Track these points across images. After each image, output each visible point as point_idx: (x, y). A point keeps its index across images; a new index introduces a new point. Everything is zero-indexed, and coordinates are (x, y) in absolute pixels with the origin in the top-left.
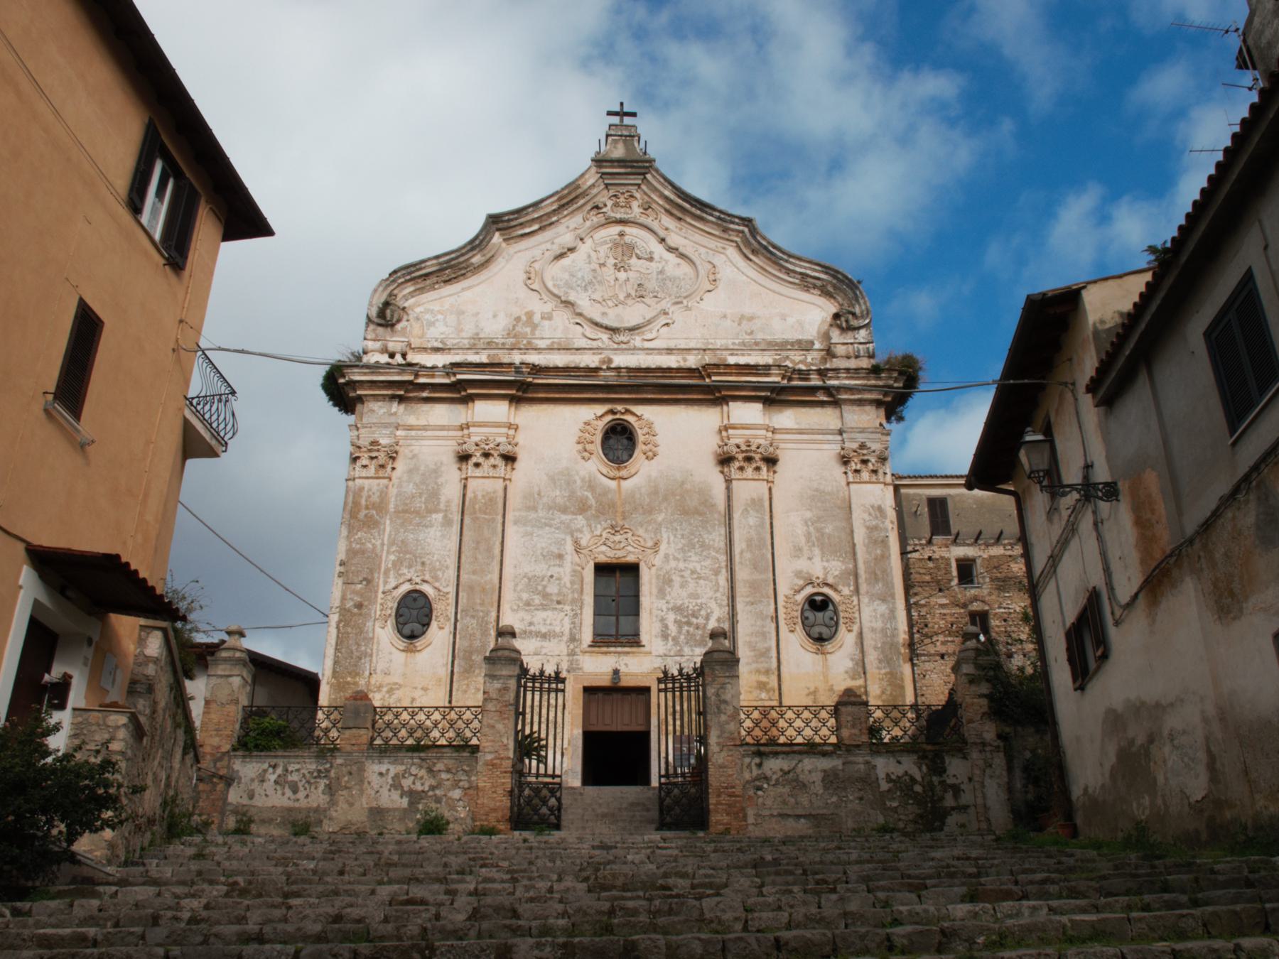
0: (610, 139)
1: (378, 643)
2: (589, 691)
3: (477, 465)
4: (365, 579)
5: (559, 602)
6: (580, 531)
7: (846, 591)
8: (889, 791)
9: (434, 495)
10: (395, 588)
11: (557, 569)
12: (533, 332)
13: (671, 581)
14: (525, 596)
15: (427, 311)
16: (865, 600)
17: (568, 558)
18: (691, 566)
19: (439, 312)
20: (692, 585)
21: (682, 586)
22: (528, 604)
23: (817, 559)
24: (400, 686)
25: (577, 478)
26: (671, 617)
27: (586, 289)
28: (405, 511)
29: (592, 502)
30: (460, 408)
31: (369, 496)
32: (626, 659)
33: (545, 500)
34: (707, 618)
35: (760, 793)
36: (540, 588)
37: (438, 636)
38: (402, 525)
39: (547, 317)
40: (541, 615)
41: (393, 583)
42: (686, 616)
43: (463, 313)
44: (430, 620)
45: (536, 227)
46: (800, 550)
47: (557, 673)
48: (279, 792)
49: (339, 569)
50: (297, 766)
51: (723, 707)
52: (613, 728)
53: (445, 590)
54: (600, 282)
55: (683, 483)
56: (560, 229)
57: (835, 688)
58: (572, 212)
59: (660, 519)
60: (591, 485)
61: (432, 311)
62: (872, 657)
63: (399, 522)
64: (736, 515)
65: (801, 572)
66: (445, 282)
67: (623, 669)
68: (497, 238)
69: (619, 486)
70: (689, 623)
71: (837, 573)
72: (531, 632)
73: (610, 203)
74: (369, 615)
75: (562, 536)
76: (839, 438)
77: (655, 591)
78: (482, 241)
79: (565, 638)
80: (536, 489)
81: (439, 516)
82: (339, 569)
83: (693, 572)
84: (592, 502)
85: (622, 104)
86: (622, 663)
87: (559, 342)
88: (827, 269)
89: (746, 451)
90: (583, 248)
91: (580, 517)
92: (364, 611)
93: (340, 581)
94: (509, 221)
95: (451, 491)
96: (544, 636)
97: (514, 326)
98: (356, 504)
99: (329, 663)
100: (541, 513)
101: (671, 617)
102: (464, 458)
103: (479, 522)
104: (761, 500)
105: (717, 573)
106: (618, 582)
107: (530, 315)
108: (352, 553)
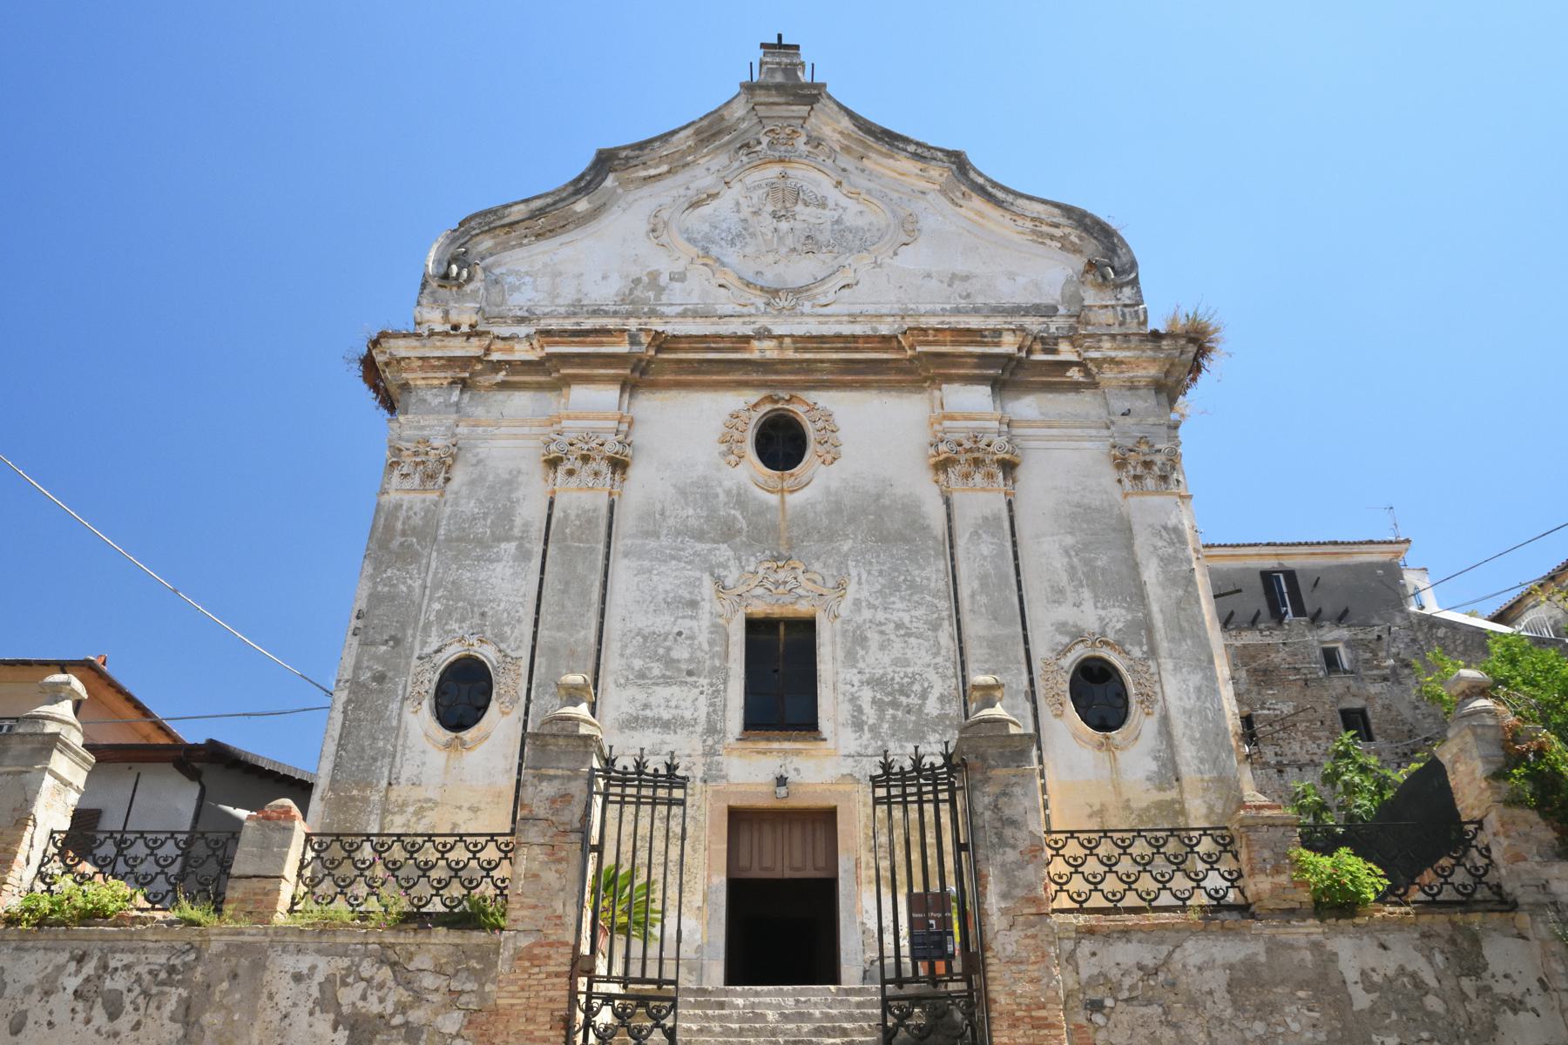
0: (765, 68)
1: (406, 736)
2: (740, 819)
3: (571, 473)
4: (392, 638)
5: (690, 673)
6: (724, 566)
7: (1137, 652)
8: (1372, 1011)
9: (506, 516)
10: (439, 651)
11: (688, 623)
12: (658, 298)
13: (865, 639)
14: (638, 664)
15: (510, 273)
16: (1167, 664)
17: (706, 606)
18: (895, 617)
19: (527, 273)
20: (898, 645)
21: (882, 648)
22: (642, 675)
23: (1088, 606)
24: (436, 803)
25: (719, 490)
26: (866, 695)
27: (733, 244)
28: (459, 539)
29: (742, 523)
30: (550, 396)
31: (409, 518)
32: (797, 762)
33: (671, 522)
34: (924, 696)
35: (1098, 1018)
36: (661, 651)
37: (500, 726)
38: (456, 558)
39: (679, 277)
40: (663, 692)
41: (434, 643)
42: (892, 692)
43: (560, 274)
44: (489, 700)
45: (664, 168)
46: (1061, 591)
47: (671, 768)
48: (81, 1016)
49: (354, 623)
50: (128, 958)
51: (1008, 832)
52: (777, 875)
53: (514, 654)
54: (753, 235)
55: (879, 497)
56: (698, 171)
57: (1134, 805)
58: (717, 148)
59: (845, 548)
60: (740, 500)
61: (517, 273)
62: (1188, 755)
63: (450, 554)
64: (961, 542)
65: (1064, 624)
66: (538, 236)
67: (792, 777)
68: (610, 181)
69: (783, 502)
70: (895, 704)
71: (1119, 626)
72: (646, 719)
73: (765, 140)
74: (395, 692)
75: (698, 574)
76: (1105, 432)
77: (840, 655)
78: (589, 183)
79: (699, 729)
80: (658, 507)
81: (511, 547)
82: (354, 623)
83: (899, 626)
84: (742, 523)
85: (780, 37)
86: (790, 768)
87: (698, 301)
88: (1068, 211)
89: (971, 450)
90: (735, 193)
91: (724, 547)
92: (388, 685)
93: (355, 641)
94: (627, 158)
95: (531, 512)
96: (666, 725)
97: (631, 291)
98: (389, 528)
99: (326, 767)
100: (664, 541)
101: (866, 695)
102: (553, 463)
103: (578, 556)
104: (997, 518)
105: (935, 627)
106: (780, 676)
107: (654, 276)
108: (375, 599)
